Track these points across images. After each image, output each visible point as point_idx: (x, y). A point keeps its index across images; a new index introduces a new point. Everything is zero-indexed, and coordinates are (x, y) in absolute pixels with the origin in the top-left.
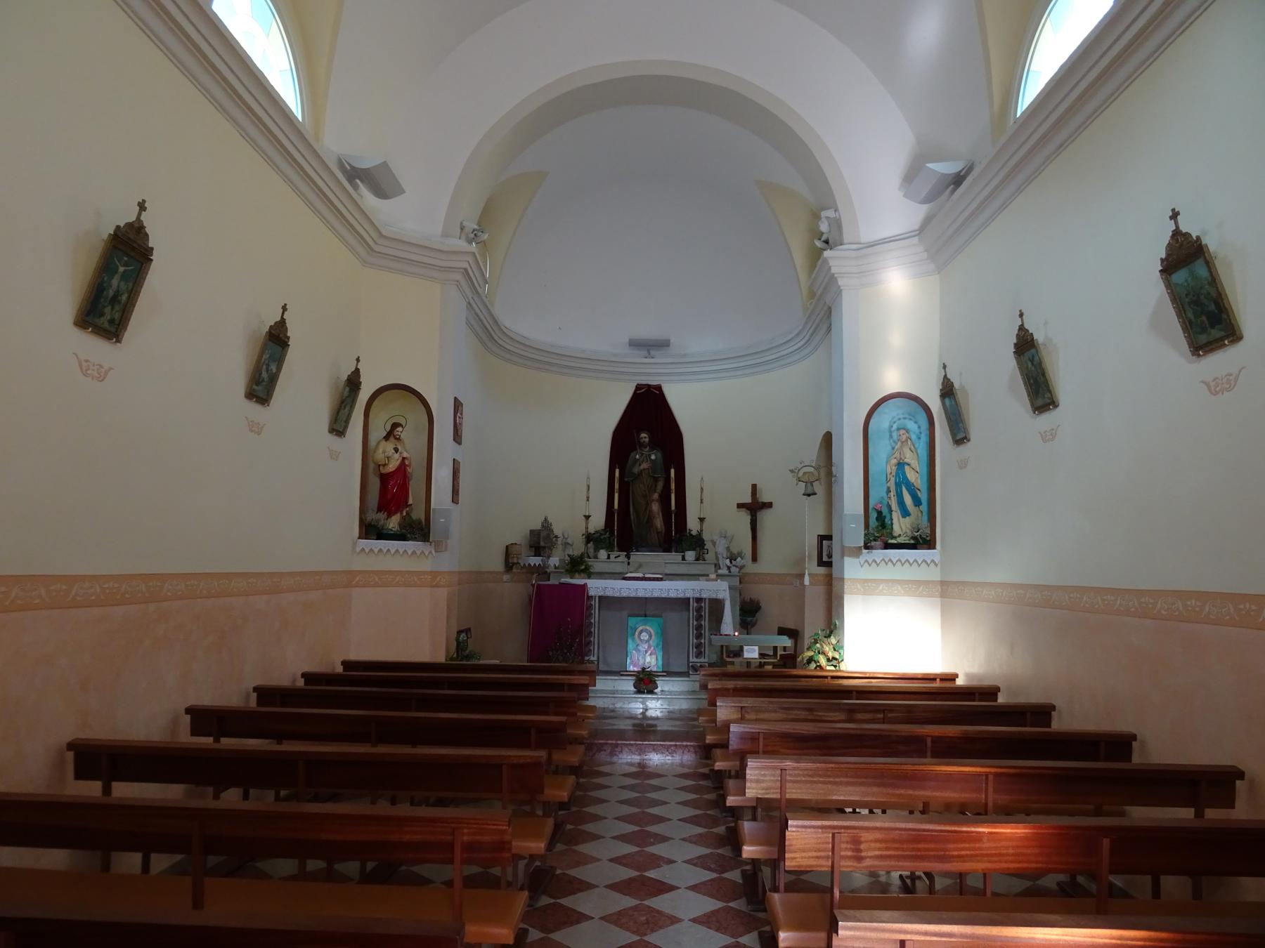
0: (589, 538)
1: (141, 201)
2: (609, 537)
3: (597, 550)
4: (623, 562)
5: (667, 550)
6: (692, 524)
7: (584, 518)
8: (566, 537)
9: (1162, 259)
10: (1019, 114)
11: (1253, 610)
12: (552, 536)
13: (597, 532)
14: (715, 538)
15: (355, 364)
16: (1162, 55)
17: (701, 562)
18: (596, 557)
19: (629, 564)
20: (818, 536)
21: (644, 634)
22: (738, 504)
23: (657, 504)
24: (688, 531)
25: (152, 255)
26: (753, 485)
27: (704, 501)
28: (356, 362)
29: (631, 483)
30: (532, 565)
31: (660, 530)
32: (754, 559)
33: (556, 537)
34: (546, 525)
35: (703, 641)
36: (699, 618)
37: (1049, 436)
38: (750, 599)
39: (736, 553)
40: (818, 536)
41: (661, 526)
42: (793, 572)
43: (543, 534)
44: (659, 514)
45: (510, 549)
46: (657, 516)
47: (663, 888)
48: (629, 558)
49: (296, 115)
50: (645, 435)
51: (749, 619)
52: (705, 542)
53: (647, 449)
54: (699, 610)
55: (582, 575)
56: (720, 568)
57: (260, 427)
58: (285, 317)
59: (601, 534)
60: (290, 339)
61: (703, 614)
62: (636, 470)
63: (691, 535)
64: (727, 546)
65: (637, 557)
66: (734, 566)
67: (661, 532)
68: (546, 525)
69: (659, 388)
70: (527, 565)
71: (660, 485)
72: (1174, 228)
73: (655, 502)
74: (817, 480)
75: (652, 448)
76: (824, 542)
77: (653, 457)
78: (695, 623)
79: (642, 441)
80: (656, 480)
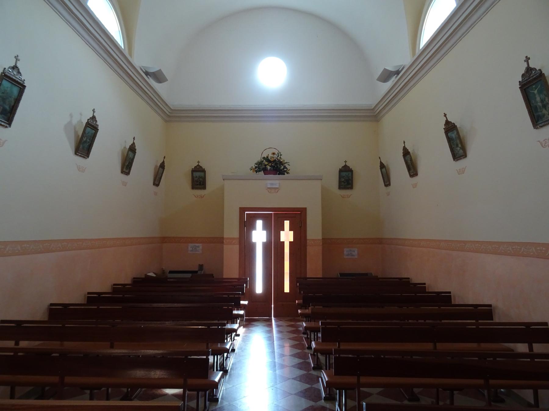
1: (16, 56)
9: (520, 82)
10: (421, 48)
11: (497, 247)
15: (163, 159)
16: (447, 55)
25: (98, 127)
28: (133, 139)
37: (461, 172)
49: (121, 46)
57: (84, 169)
58: (134, 142)
60: (99, 126)
72: (446, 119)
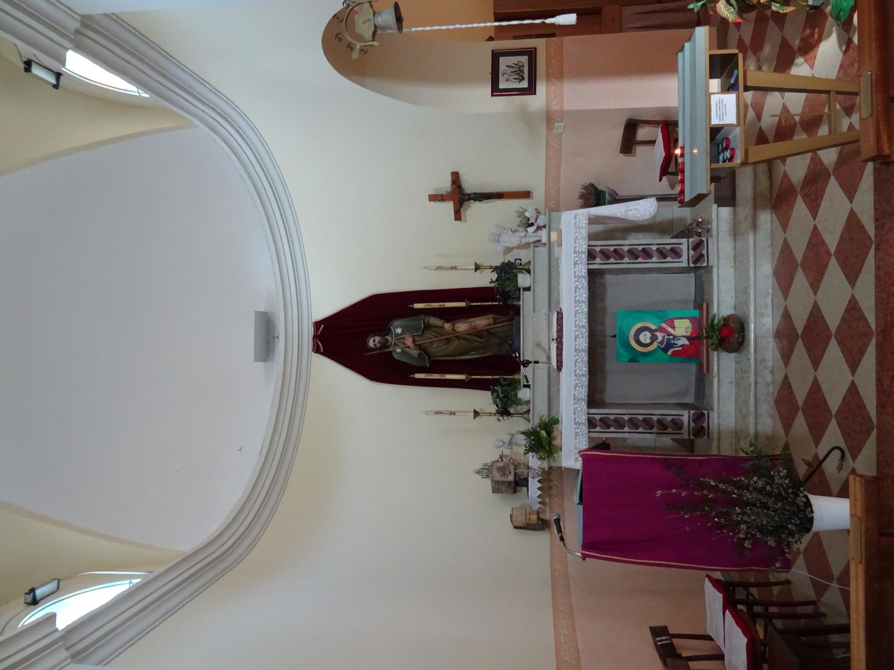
0: (504, 412)
2: (501, 387)
3: (518, 402)
5: (517, 310)
6: (485, 279)
7: (477, 418)
8: (501, 443)
12: (501, 464)
13: (495, 402)
14: (500, 248)
17: (531, 267)
18: (528, 402)
19: (537, 362)
20: (492, 95)
21: (648, 341)
22: (456, 219)
23: (458, 325)
24: (493, 285)
26: (430, 200)
27: (454, 265)
29: (432, 358)
30: (539, 485)
31: (491, 321)
32: (526, 195)
33: (501, 457)
34: (486, 471)
35: (654, 248)
36: (618, 254)
39: (519, 219)
40: (492, 95)
42: (543, 130)
43: (498, 477)
44: (471, 322)
45: (516, 524)
46: (473, 324)
47: (816, 314)
48: (528, 362)
50: (372, 340)
51: (607, 196)
52: (506, 262)
53: (388, 337)
54: (606, 255)
55: (555, 433)
56: (539, 241)
59: (498, 396)
61: (612, 249)
62: (415, 353)
63: (497, 280)
64: (510, 233)
65: (527, 351)
66: (536, 221)
67: (494, 318)
68: (486, 471)
69: (317, 324)
70: (540, 500)
71: (434, 321)
73: (456, 329)
74: (372, 6)
75: (389, 332)
76: (501, 87)
77: (399, 331)
78: (626, 260)
79: (378, 346)
80: (427, 326)
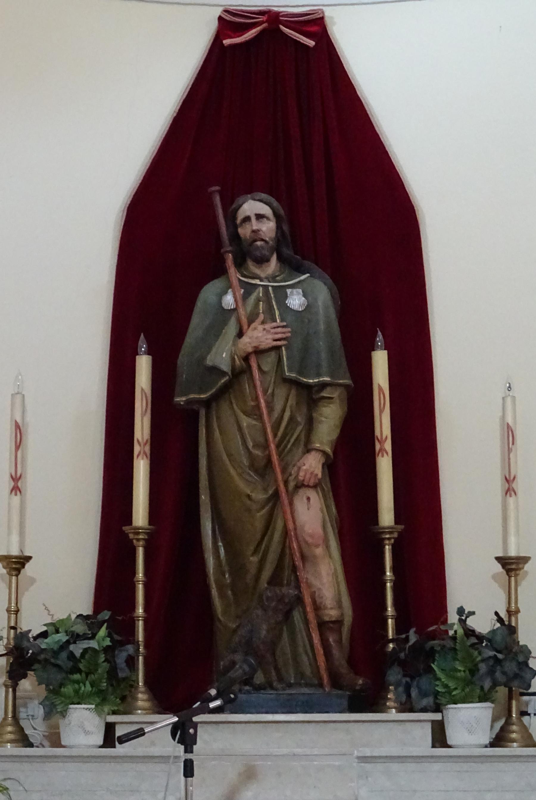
2: (106, 650)
4: (164, 759)
17: (515, 749)
24: (453, 618)
27: (519, 485)
29: (203, 412)
31: (332, 614)
38: (39, 684)
41: (328, 325)
46: (319, 551)
50: (266, 210)
59: (75, 638)
63: (470, 633)
79: (245, 232)
